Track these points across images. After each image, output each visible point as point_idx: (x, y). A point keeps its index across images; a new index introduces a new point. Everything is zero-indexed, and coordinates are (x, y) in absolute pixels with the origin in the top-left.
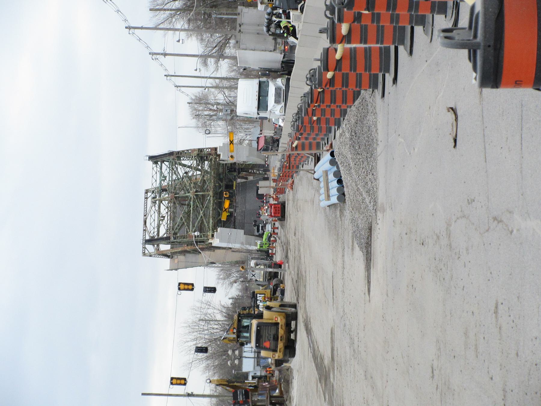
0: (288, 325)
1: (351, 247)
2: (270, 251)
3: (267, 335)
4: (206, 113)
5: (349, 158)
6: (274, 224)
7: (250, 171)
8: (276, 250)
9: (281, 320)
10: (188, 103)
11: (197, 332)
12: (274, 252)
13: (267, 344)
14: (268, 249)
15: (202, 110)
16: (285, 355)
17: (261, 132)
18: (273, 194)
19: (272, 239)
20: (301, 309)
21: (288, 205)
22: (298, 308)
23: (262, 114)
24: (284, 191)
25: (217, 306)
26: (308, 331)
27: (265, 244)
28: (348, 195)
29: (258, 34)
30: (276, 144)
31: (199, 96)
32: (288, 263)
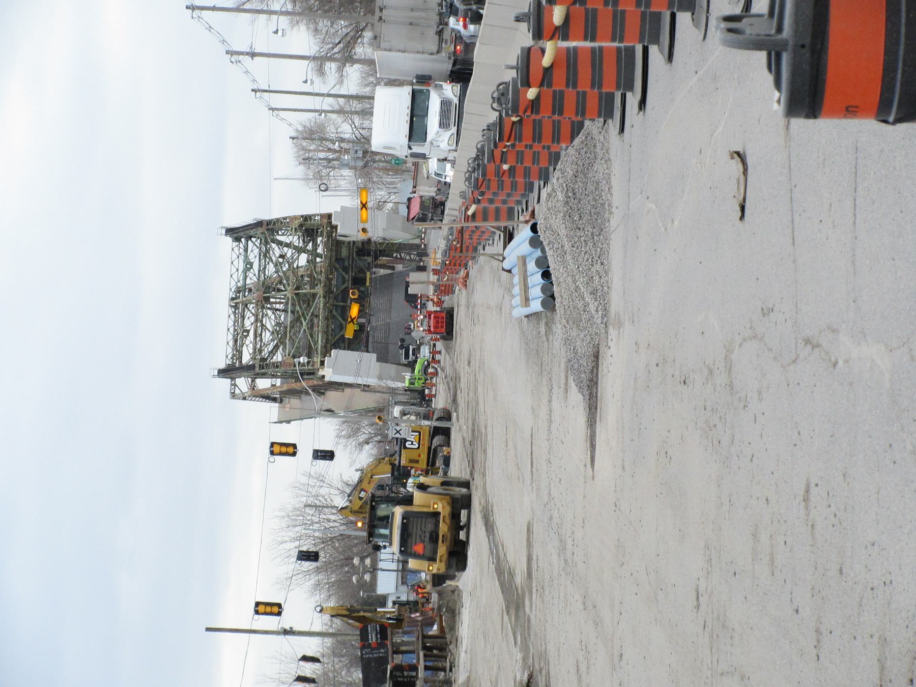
0: (455, 516)
1: (563, 386)
2: (427, 392)
3: (419, 531)
4: (322, 155)
8: (438, 389)
9: (444, 507)
10: (291, 138)
12: (433, 393)
13: (419, 548)
14: (423, 387)
16: (449, 566)
17: (414, 189)
18: (434, 294)
19: (430, 370)
21: (457, 313)
22: (473, 488)
23: (417, 149)
25: (335, 482)
26: (489, 526)
28: (560, 298)
29: (411, 24)
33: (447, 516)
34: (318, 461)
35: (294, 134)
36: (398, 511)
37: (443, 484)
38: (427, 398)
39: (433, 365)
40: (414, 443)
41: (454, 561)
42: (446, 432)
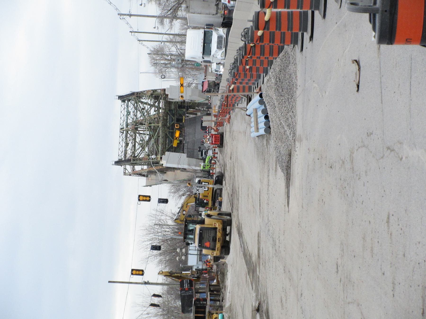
1: (274, 169)
2: (211, 171)
4: (162, 62)
6: (215, 150)
7: (196, 108)
9: (219, 225)
11: (152, 234)
12: (214, 172)
13: (207, 244)
15: (159, 60)
16: (221, 253)
17: (205, 78)
19: (213, 162)
20: (234, 217)
22: (233, 216)
24: (223, 124)
26: (240, 234)
27: (207, 165)
32: (225, 181)
33: (221, 229)
35: (149, 52)
36: (198, 227)
37: (219, 214)
40: (206, 188)
41: (224, 250)
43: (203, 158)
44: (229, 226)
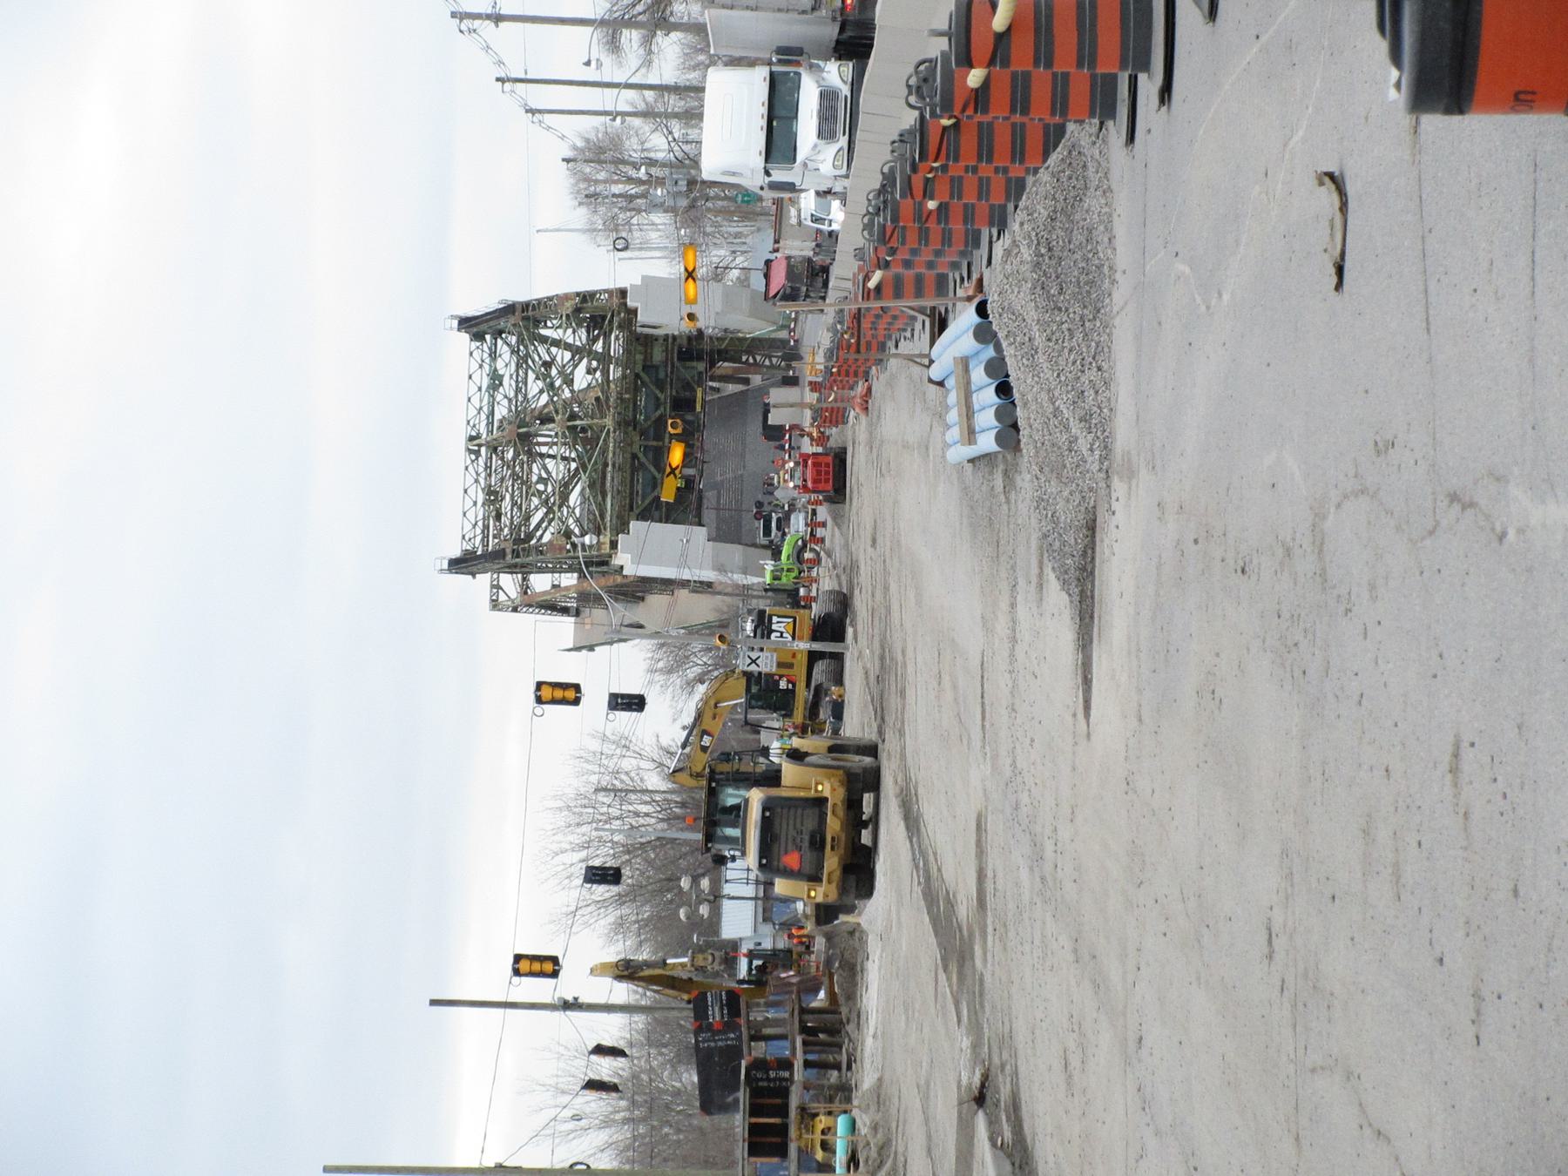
0: (853, 804)
1: (1034, 580)
2: (802, 592)
3: (792, 832)
5: (1029, 321)
6: (814, 512)
9: (833, 790)
10: (564, 160)
12: (814, 593)
13: (792, 860)
15: (605, 182)
16: (843, 890)
17: (776, 246)
18: (812, 425)
19: (808, 555)
22: (883, 756)
26: (912, 822)
28: (1028, 430)
30: (820, 280)
31: (598, 139)
33: (840, 804)
34: (617, 713)
35: (569, 154)
36: (756, 796)
37: (832, 749)
38: (803, 603)
39: (813, 546)
40: (784, 635)
42: (838, 658)
43: (771, 542)
44: (869, 791)
